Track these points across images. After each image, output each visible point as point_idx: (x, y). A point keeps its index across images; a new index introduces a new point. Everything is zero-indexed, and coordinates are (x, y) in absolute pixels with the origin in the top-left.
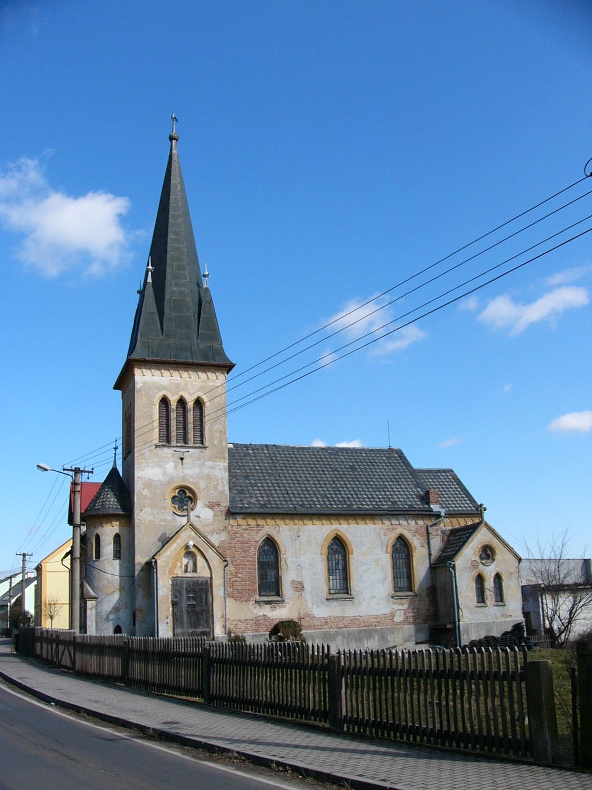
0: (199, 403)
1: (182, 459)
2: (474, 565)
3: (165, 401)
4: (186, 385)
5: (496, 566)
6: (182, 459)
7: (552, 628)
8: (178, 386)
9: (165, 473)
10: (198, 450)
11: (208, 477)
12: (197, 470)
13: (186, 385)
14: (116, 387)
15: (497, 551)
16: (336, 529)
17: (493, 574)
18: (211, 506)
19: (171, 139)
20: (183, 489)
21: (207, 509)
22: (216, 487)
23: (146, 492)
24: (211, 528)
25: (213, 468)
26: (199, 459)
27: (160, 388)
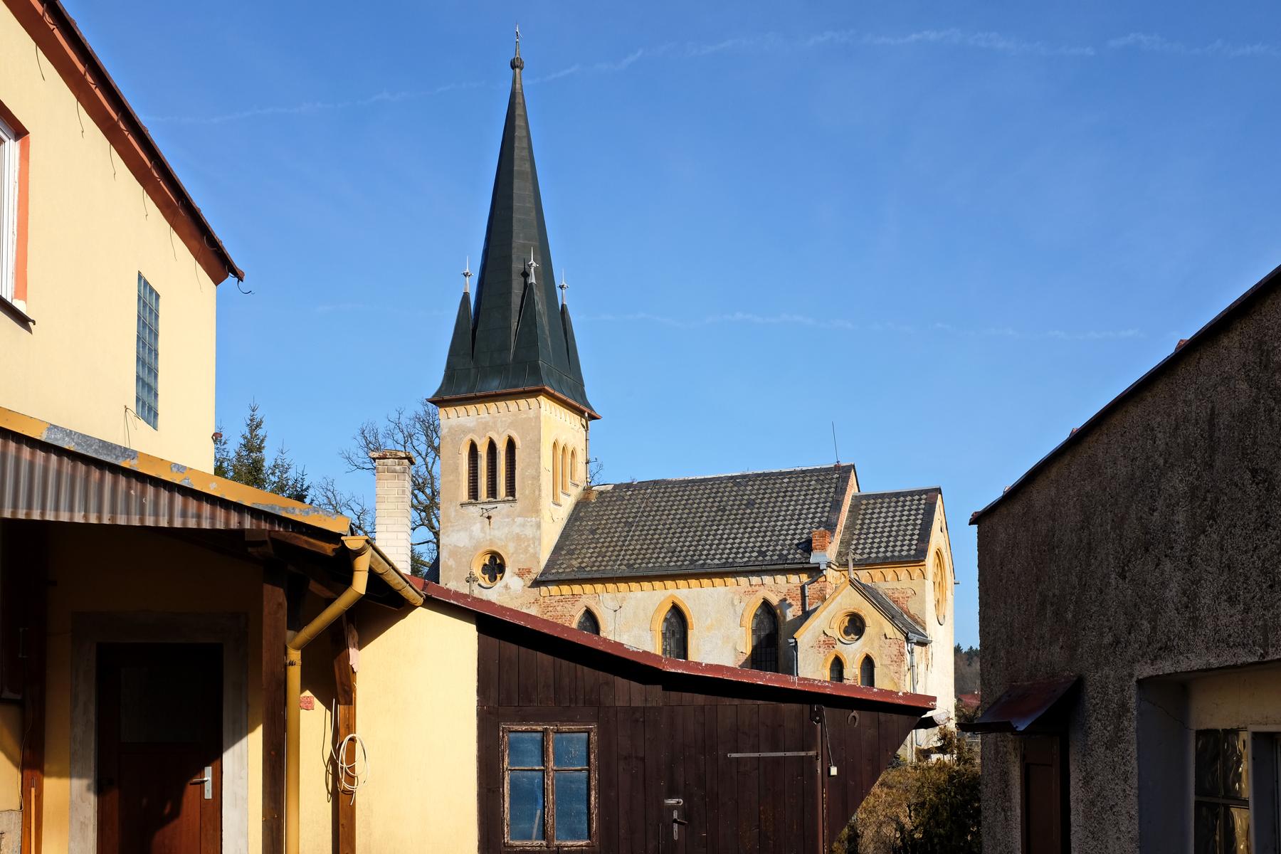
0: (511, 445)
1: (489, 518)
2: (829, 643)
3: (473, 448)
4: (495, 423)
5: (864, 645)
6: (489, 518)
7: (329, 707)
8: (486, 427)
9: (471, 538)
10: (508, 505)
11: (518, 538)
12: (506, 530)
13: (495, 423)
14: (977, 519)
15: (868, 621)
16: (671, 596)
17: (860, 658)
18: (521, 574)
19: (513, 66)
20: (494, 556)
21: (516, 578)
22: (526, 551)
23: (451, 562)
24: (520, 601)
25: (524, 525)
26: (508, 516)
27: (465, 431)
